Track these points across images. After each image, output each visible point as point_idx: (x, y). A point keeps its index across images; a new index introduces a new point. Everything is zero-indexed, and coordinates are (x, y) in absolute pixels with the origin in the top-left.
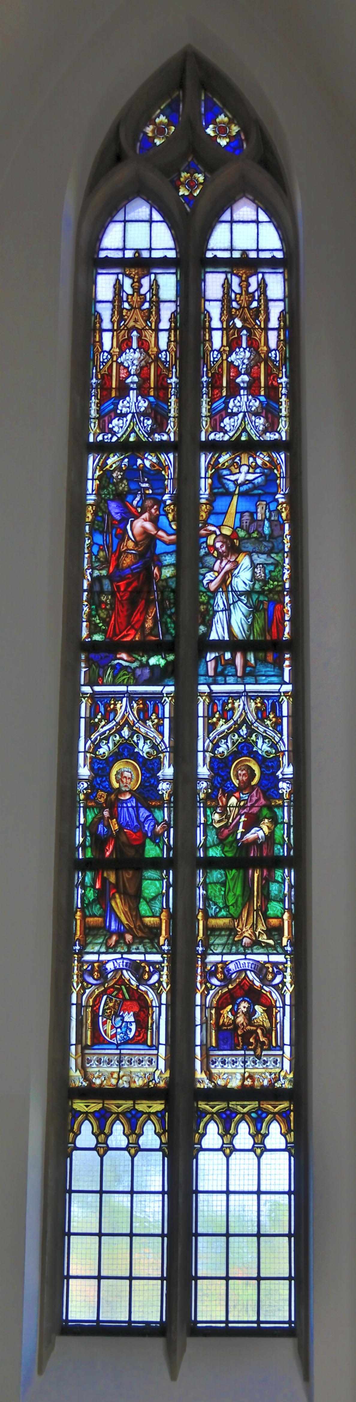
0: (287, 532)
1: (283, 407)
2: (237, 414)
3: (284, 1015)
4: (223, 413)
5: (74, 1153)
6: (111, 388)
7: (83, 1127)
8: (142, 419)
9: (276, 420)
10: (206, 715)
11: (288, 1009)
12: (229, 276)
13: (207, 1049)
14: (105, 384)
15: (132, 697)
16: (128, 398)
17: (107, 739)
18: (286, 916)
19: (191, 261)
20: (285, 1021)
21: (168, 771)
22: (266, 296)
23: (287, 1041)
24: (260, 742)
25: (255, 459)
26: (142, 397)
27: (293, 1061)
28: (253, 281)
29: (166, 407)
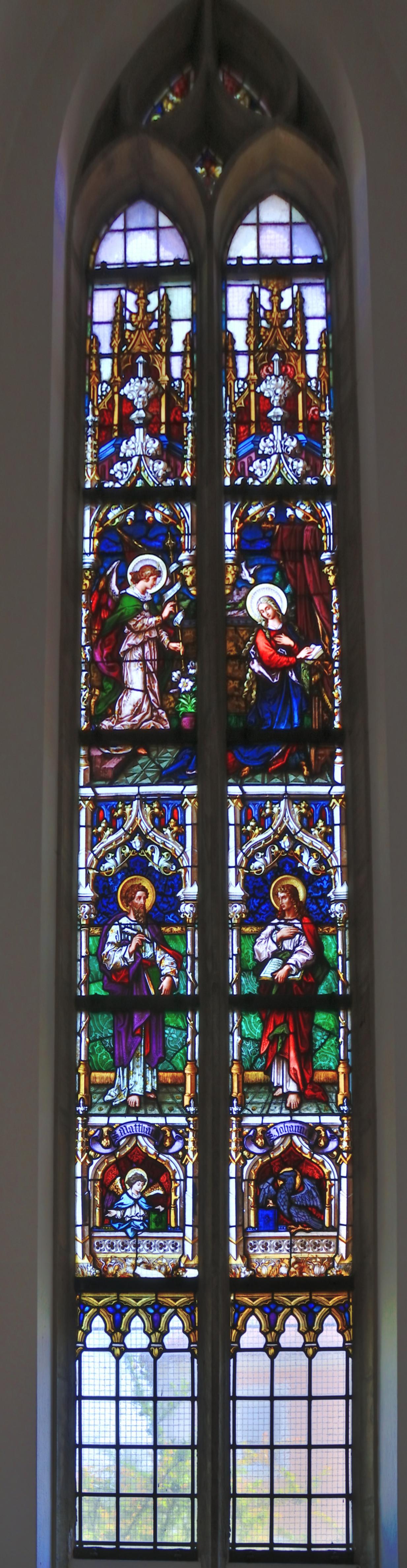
0: (335, 599)
1: (189, 448)
2: (269, 456)
3: (340, 1189)
4: (253, 455)
5: (239, 1354)
6: (113, 425)
7: (249, 1323)
8: (290, 460)
9: (179, 463)
10: (238, 822)
11: (344, 1182)
12: (256, 289)
13: (243, 1230)
14: (105, 421)
15: (145, 799)
16: (271, 436)
17: (114, 851)
18: (341, 1069)
19: (208, 271)
20: (187, 1197)
21: (191, 890)
22: (302, 313)
23: (189, 1220)
24: (306, 855)
25: (153, 513)
26: (151, 437)
27: (350, 1245)
28: (287, 295)
29: (319, 445)
